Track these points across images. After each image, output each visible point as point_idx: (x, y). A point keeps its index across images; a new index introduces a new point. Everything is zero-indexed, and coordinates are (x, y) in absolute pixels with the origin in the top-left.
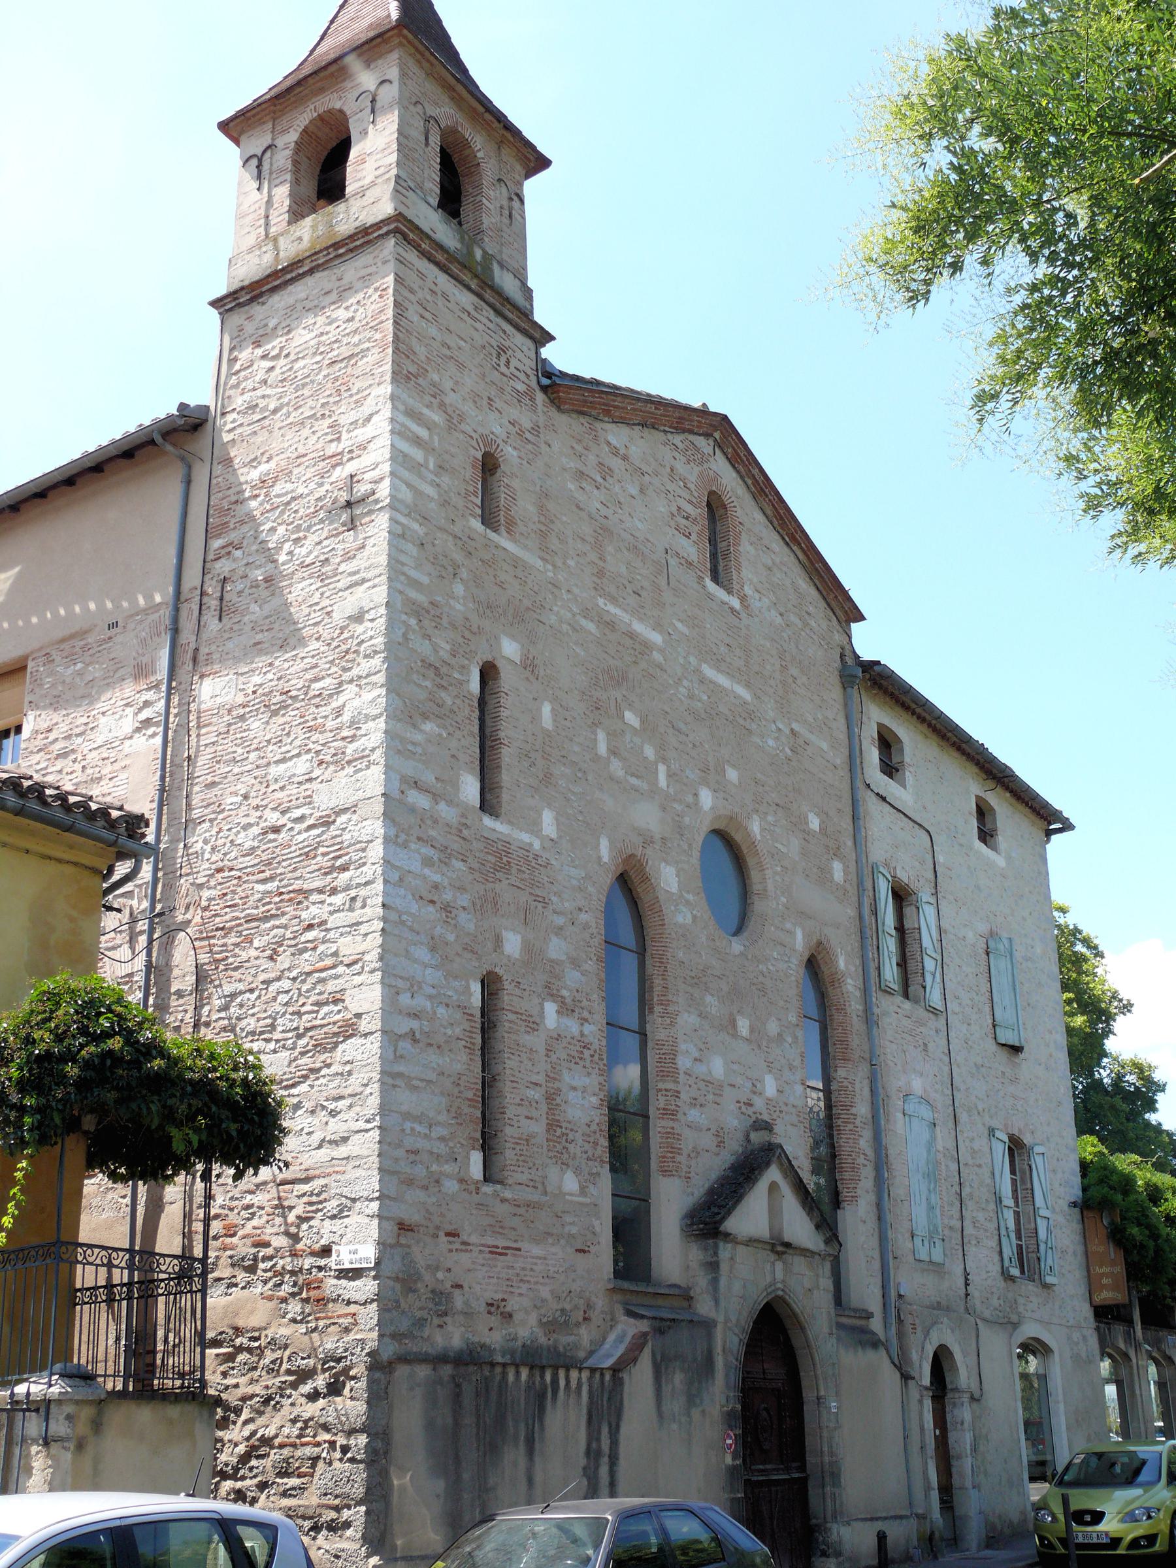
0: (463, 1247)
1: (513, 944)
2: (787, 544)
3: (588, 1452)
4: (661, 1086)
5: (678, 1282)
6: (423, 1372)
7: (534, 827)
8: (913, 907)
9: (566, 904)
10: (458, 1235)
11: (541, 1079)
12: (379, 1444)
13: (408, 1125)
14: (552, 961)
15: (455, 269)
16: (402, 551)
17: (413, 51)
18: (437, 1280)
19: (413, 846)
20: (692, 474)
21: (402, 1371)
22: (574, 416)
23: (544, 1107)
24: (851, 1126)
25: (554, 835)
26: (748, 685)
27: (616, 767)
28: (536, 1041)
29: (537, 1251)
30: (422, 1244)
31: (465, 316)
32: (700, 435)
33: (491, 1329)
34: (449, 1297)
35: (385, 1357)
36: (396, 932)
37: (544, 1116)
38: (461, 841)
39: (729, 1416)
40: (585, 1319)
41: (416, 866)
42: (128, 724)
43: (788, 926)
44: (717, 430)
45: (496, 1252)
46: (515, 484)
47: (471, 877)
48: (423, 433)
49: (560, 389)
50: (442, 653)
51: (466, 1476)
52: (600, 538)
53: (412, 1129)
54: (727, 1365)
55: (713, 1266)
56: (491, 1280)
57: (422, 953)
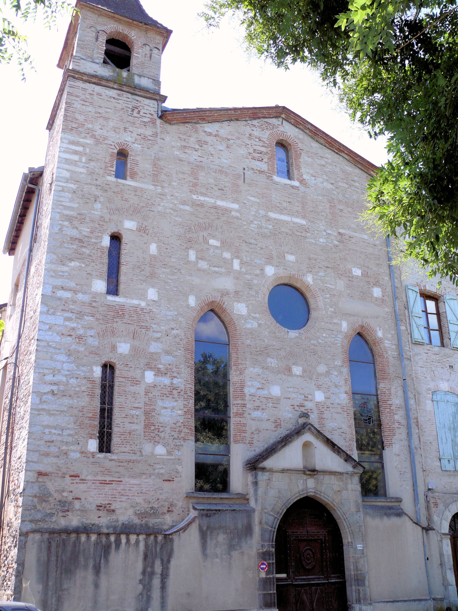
0: (81, 482)
1: (124, 348)
2: (337, 153)
3: (144, 573)
4: (235, 402)
5: (241, 492)
6: (38, 536)
7: (143, 296)
8: (442, 303)
9: (162, 328)
10: (79, 476)
11: (141, 405)
12: (20, 568)
13: (47, 431)
14: (152, 353)
15: (103, 83)
16: (61, 197)
17: (88, 9)
18: (63, 496)
19: (59, 314)
20: (266, 135)
21: (31, 536)
22: (182, 125)
23: (143, 418)
24: (388, 410)
25: (156, 298)
26: (304, 217)
27: (203, 265)
28: (141, 389)
29: (133, 481)
30: (53, 481)
31: (112, 100)
32: (272, 118)
33: (100, 517)
34: (70, 503)
35: (25, 530)
36: (45, 350)
37: (143, 422)
38: (92, 308)
39: (264, 556)
40: (168, 511)
41: (60, 321)
43: (335, 321)
44: (282, 113)
46: (138, 158)
47: (97, 323)
48: (80, 149)
49: (166, 116)
50: (84, 233)
51: (50, 583)
52: (195, 171)
53: (50, 432)
54: (263, 531)
55: (256, 483)
56: (101, 496)
57: (63, 358)
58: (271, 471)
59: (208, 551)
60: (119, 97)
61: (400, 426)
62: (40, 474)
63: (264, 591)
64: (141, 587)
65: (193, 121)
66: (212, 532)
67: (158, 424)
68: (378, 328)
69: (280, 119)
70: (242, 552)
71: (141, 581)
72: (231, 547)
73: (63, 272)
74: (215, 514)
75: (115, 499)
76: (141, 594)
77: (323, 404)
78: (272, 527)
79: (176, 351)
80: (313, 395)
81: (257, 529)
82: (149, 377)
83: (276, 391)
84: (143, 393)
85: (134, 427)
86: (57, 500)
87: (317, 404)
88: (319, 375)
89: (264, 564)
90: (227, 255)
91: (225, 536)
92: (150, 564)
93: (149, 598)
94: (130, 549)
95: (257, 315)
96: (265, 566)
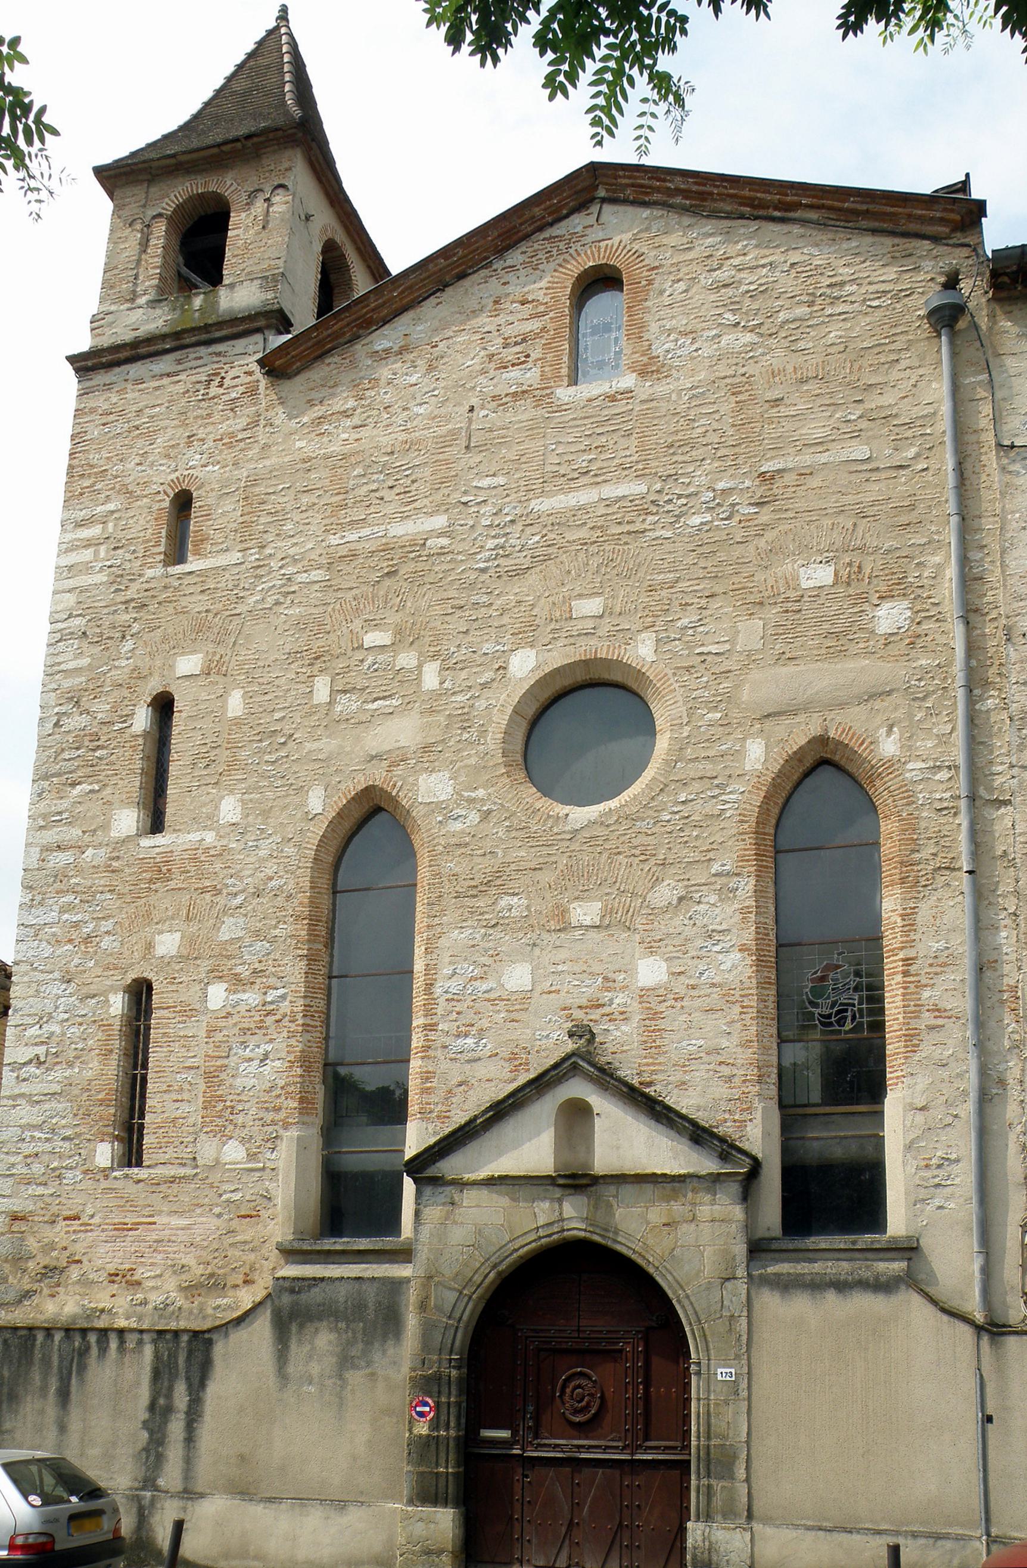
0: (83, 1228)
3: (152, 1407)
7: (210, 821)
27: (347, 704)
40: (245, 1282)
42: (474, 362)
45: (122, 1228)
53: (32, 1137)
54: (427, 1329)
57: (57, 989)
58: (461, 1185)
59: (291, 1369)
60: (180, 367)
61: (940, 1022)
62: (15, 1218)
63: (419, 1465)
64: (146, 1435)
65: (341, 340)
66: (301, 1326)
67: (231, 1097)
68: (883, 731)
69: (595, 208)
70: (373, 1374)
71: (145, 1424)
72: (345, 1362)
73: (60, 813)
74: (310, 1287)
75: (143, 1260)
76: (146, 1450)
77: (662, 992)
78: (449, 1317)
79: (276, 927)
80: (630, 970)
81: (412, 1322)
82: (217, 995)
83: (518, 977)
84: (203, 1034)
85: (185, 1107)
86: (41, 1265)
87: (644, 994)
88: (654, 913)
89: (426, 1404)
90: (407, 659)
91: (333, 1336)
92: (164, 1391)
93: (160, 1458)
94: (126, 1360)
95: (481, 793)
96: (427, 1409)
